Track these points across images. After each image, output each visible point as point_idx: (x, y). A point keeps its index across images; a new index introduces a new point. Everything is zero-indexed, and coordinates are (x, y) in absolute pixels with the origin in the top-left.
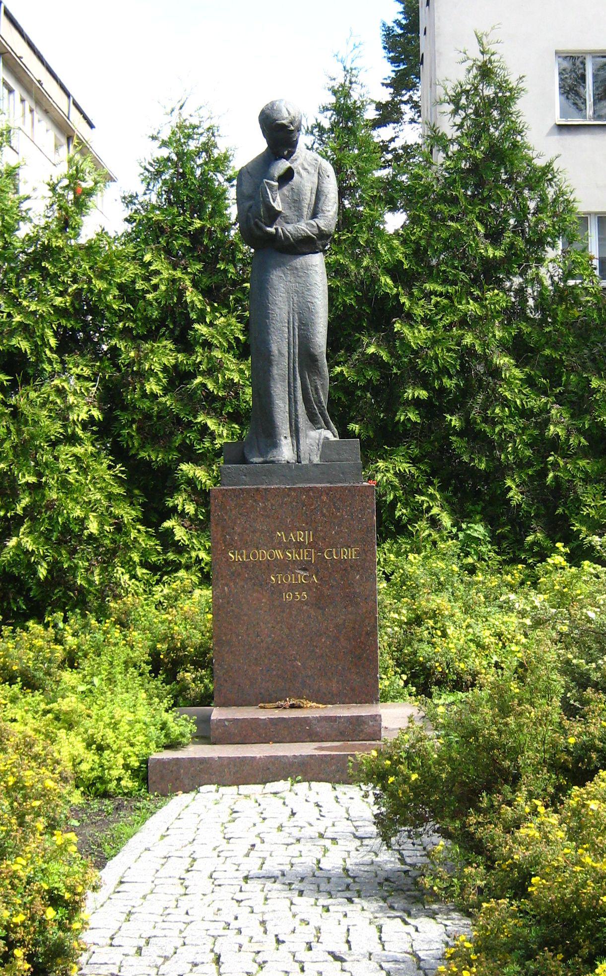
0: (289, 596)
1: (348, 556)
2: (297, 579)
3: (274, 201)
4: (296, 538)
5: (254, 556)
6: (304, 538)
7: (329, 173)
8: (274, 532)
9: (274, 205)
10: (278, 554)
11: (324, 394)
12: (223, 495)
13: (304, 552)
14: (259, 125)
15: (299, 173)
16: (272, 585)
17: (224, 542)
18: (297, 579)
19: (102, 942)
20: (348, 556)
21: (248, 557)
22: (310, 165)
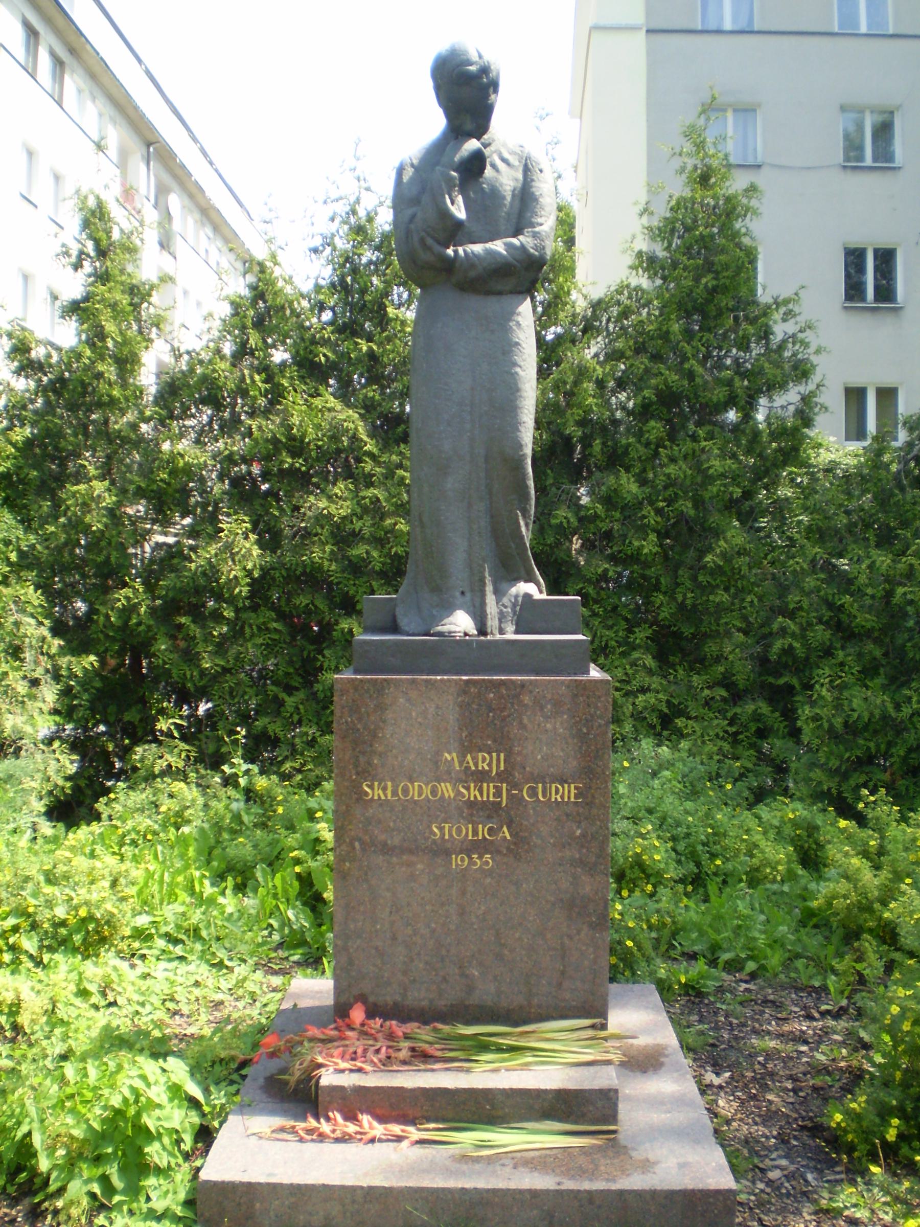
0: (462, 860)
1: (562, 797)
2: (475, 833)
3: (453, 203)
4: (476, 765)
5: (406, 791)
6: (490, 765)
7: (542, 166)
8: (438, 753)
9: (453, 209)
10: (447, 790)
11: (527, 525)
12: (356, 689)
13: (489, 789)
14: (429, 84)
15: (493, 166)
16: (434, 842)
17: (356, 766)
18: (475, 833)
19: (165, 1079)
20: (562, 797)
21: (394, 793)
22: (513, 153)
